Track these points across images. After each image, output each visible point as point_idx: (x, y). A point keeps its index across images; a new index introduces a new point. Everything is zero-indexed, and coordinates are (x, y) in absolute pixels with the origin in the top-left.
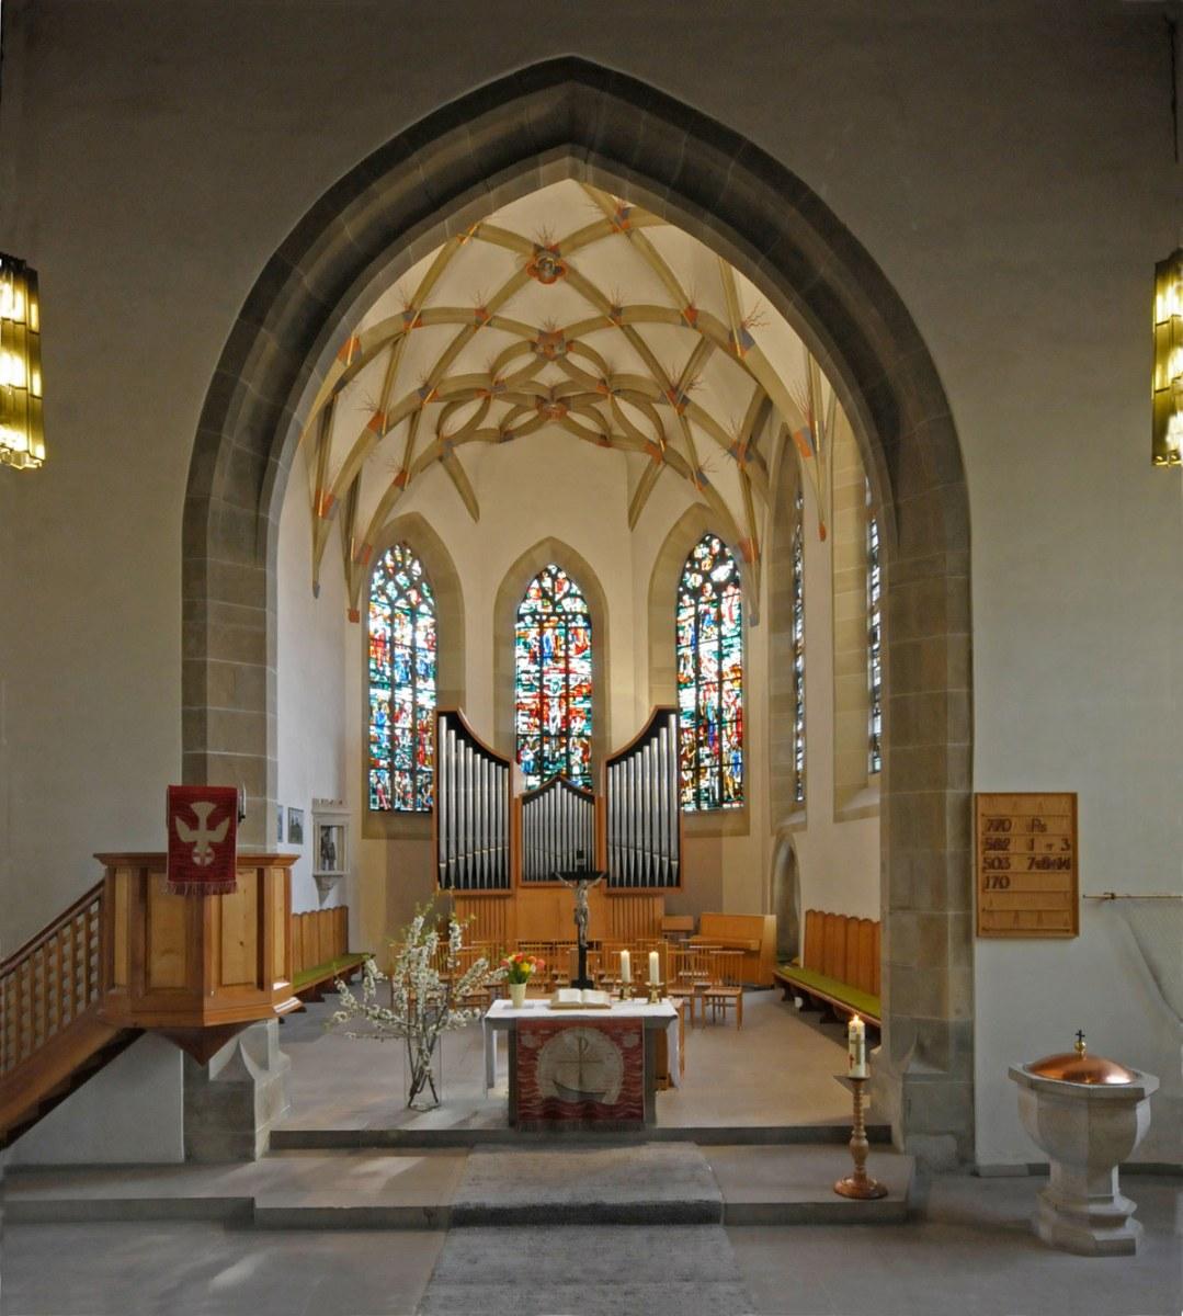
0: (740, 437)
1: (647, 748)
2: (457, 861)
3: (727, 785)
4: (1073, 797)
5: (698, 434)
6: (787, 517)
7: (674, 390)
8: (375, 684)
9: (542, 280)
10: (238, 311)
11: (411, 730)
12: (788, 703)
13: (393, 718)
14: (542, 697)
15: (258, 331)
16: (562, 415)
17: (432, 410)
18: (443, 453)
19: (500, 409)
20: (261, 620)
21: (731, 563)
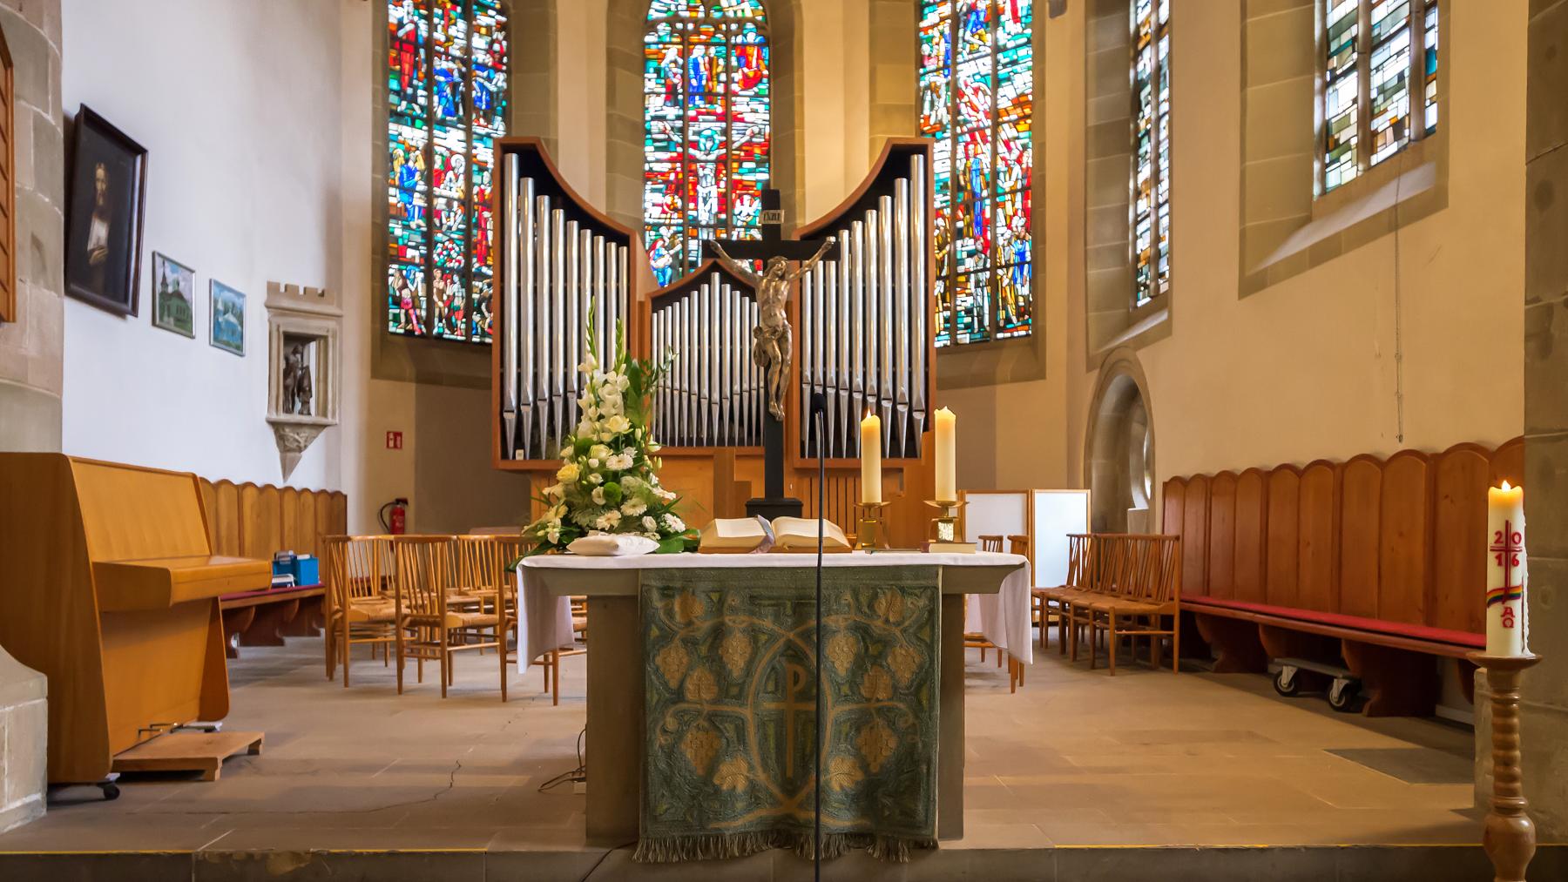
2: (536, 410)
3: (1004, 299)
8: (399, 117)
12: (1117, 138)
13: (433, 178)
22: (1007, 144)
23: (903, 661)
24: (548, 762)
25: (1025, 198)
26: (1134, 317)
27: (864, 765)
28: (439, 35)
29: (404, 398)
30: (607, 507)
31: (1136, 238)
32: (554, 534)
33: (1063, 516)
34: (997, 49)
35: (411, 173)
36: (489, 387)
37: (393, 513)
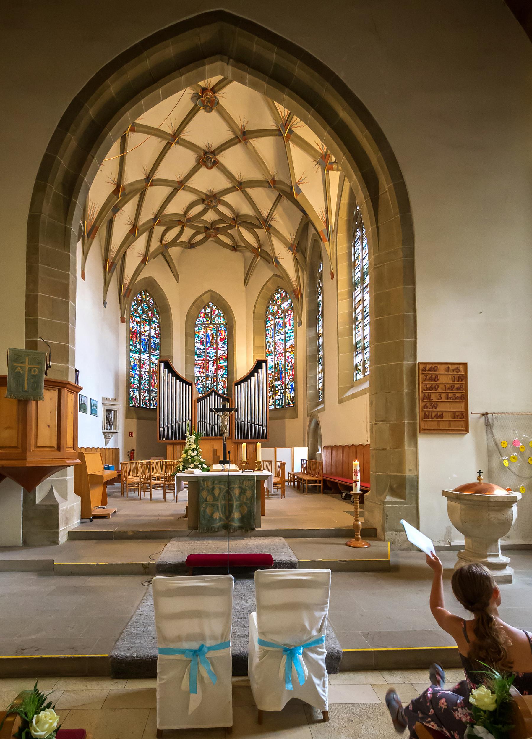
0: (294, 242)
1: (253, 378)
2: (168, 427)
4: (465, 365)
5: (276, 242)
6: (314, 277)
7: (266, 221)
8: (132, 351)
9: (208, 168)
10: (57, 124)
11: (148, 372)
13: (141, 366)
14: (205, 360)
15: (66, 134)
16: (215, 236)
17: (159, 230)
18: (163, 251)
19: (188, 232)
20: (67, 277)
21: (290, 300)
22: (288, 357)
23: (249, 494)
24: (178, 515)
25: (292, 371)
26: (318, 405)
27: (241, 514)
28: (143, 330)
29: (133, 423)
30: (191, 463)
31: (319, 384)
32: (181, 469)
33: (302, 453)
34: (286, 333)
35: (135, 366)
36: (156, 420)
37: (131, 453)
